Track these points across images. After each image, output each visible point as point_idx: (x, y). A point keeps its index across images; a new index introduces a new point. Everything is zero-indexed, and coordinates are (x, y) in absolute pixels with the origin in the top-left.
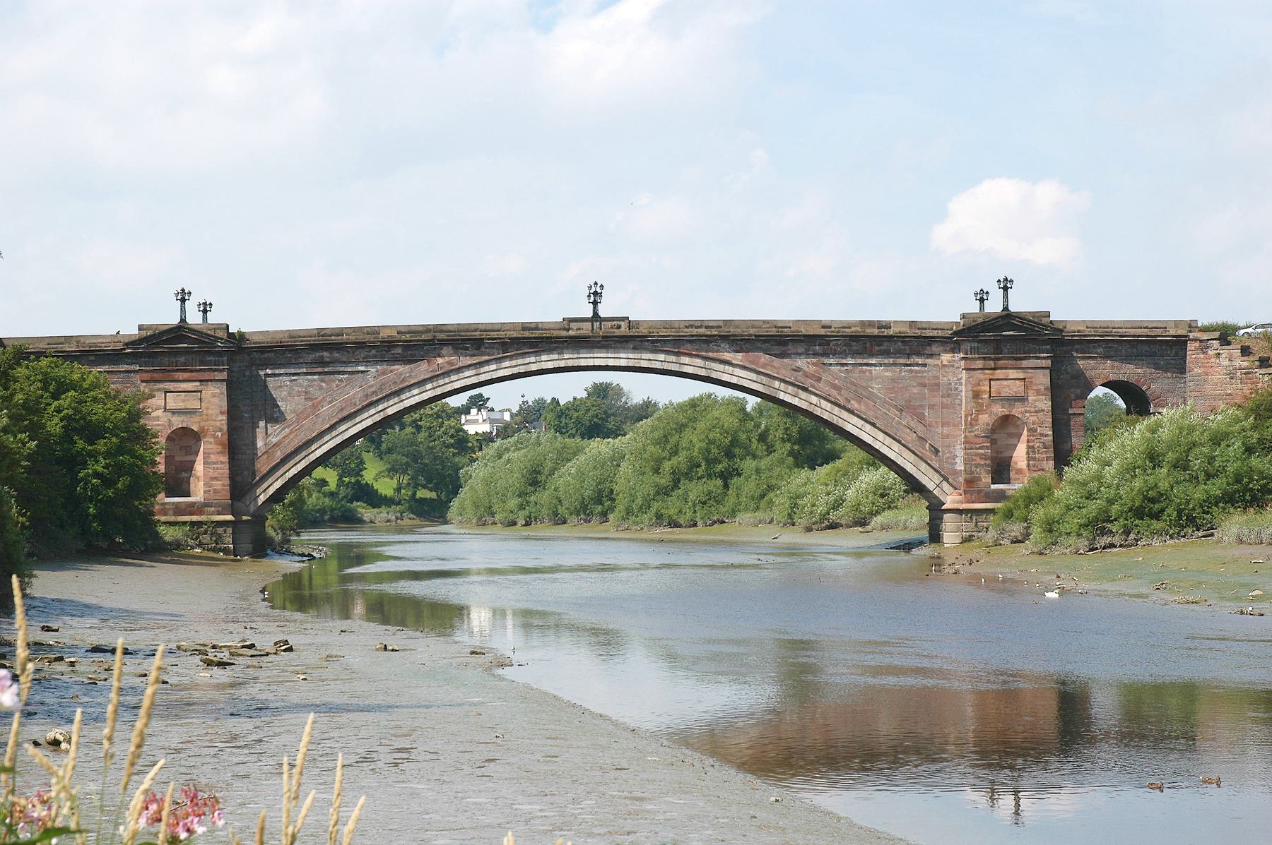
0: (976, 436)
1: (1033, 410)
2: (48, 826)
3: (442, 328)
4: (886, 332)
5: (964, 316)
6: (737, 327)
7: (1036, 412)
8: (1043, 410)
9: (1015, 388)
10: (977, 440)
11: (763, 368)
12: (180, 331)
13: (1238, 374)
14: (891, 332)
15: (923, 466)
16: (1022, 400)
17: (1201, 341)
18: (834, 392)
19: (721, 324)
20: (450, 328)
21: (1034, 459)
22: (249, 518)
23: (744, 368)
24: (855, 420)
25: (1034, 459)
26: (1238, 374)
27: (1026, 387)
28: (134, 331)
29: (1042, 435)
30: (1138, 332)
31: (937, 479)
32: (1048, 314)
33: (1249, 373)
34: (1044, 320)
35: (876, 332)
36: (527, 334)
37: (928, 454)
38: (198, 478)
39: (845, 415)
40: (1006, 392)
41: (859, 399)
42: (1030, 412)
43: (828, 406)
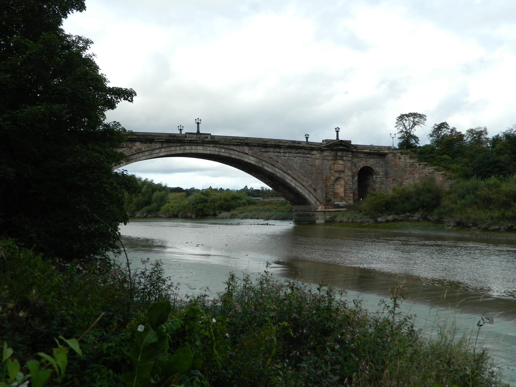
0: (330, 184)
1: (346, 175)
3: (136, 134)
4: (300, 145)
6: (250, 140)
7: (347, 176)
8: (349, 176)
9: (341, 168)
10: (330, 186)
11: (259, 156)
15: (311, 195)
17: (394, 153)
18: (283, 168)
19: (244, 139)
20: (139, 134)
21: (347, 193)
23: (252, 156)
24: (289, 178)
25: (347, 193)
26: (408, 165)
29: (349, 184)
31: (315, 200)
32: (350, 142)
33: (412, 164)
35: (297, 145)
36: (171, 138)
37: (312, 191)
38: (376, 266)
39: (286, 176)
40: (339, 169)
41: (291, 170)
42: (346, 176)
43: (281, 172)
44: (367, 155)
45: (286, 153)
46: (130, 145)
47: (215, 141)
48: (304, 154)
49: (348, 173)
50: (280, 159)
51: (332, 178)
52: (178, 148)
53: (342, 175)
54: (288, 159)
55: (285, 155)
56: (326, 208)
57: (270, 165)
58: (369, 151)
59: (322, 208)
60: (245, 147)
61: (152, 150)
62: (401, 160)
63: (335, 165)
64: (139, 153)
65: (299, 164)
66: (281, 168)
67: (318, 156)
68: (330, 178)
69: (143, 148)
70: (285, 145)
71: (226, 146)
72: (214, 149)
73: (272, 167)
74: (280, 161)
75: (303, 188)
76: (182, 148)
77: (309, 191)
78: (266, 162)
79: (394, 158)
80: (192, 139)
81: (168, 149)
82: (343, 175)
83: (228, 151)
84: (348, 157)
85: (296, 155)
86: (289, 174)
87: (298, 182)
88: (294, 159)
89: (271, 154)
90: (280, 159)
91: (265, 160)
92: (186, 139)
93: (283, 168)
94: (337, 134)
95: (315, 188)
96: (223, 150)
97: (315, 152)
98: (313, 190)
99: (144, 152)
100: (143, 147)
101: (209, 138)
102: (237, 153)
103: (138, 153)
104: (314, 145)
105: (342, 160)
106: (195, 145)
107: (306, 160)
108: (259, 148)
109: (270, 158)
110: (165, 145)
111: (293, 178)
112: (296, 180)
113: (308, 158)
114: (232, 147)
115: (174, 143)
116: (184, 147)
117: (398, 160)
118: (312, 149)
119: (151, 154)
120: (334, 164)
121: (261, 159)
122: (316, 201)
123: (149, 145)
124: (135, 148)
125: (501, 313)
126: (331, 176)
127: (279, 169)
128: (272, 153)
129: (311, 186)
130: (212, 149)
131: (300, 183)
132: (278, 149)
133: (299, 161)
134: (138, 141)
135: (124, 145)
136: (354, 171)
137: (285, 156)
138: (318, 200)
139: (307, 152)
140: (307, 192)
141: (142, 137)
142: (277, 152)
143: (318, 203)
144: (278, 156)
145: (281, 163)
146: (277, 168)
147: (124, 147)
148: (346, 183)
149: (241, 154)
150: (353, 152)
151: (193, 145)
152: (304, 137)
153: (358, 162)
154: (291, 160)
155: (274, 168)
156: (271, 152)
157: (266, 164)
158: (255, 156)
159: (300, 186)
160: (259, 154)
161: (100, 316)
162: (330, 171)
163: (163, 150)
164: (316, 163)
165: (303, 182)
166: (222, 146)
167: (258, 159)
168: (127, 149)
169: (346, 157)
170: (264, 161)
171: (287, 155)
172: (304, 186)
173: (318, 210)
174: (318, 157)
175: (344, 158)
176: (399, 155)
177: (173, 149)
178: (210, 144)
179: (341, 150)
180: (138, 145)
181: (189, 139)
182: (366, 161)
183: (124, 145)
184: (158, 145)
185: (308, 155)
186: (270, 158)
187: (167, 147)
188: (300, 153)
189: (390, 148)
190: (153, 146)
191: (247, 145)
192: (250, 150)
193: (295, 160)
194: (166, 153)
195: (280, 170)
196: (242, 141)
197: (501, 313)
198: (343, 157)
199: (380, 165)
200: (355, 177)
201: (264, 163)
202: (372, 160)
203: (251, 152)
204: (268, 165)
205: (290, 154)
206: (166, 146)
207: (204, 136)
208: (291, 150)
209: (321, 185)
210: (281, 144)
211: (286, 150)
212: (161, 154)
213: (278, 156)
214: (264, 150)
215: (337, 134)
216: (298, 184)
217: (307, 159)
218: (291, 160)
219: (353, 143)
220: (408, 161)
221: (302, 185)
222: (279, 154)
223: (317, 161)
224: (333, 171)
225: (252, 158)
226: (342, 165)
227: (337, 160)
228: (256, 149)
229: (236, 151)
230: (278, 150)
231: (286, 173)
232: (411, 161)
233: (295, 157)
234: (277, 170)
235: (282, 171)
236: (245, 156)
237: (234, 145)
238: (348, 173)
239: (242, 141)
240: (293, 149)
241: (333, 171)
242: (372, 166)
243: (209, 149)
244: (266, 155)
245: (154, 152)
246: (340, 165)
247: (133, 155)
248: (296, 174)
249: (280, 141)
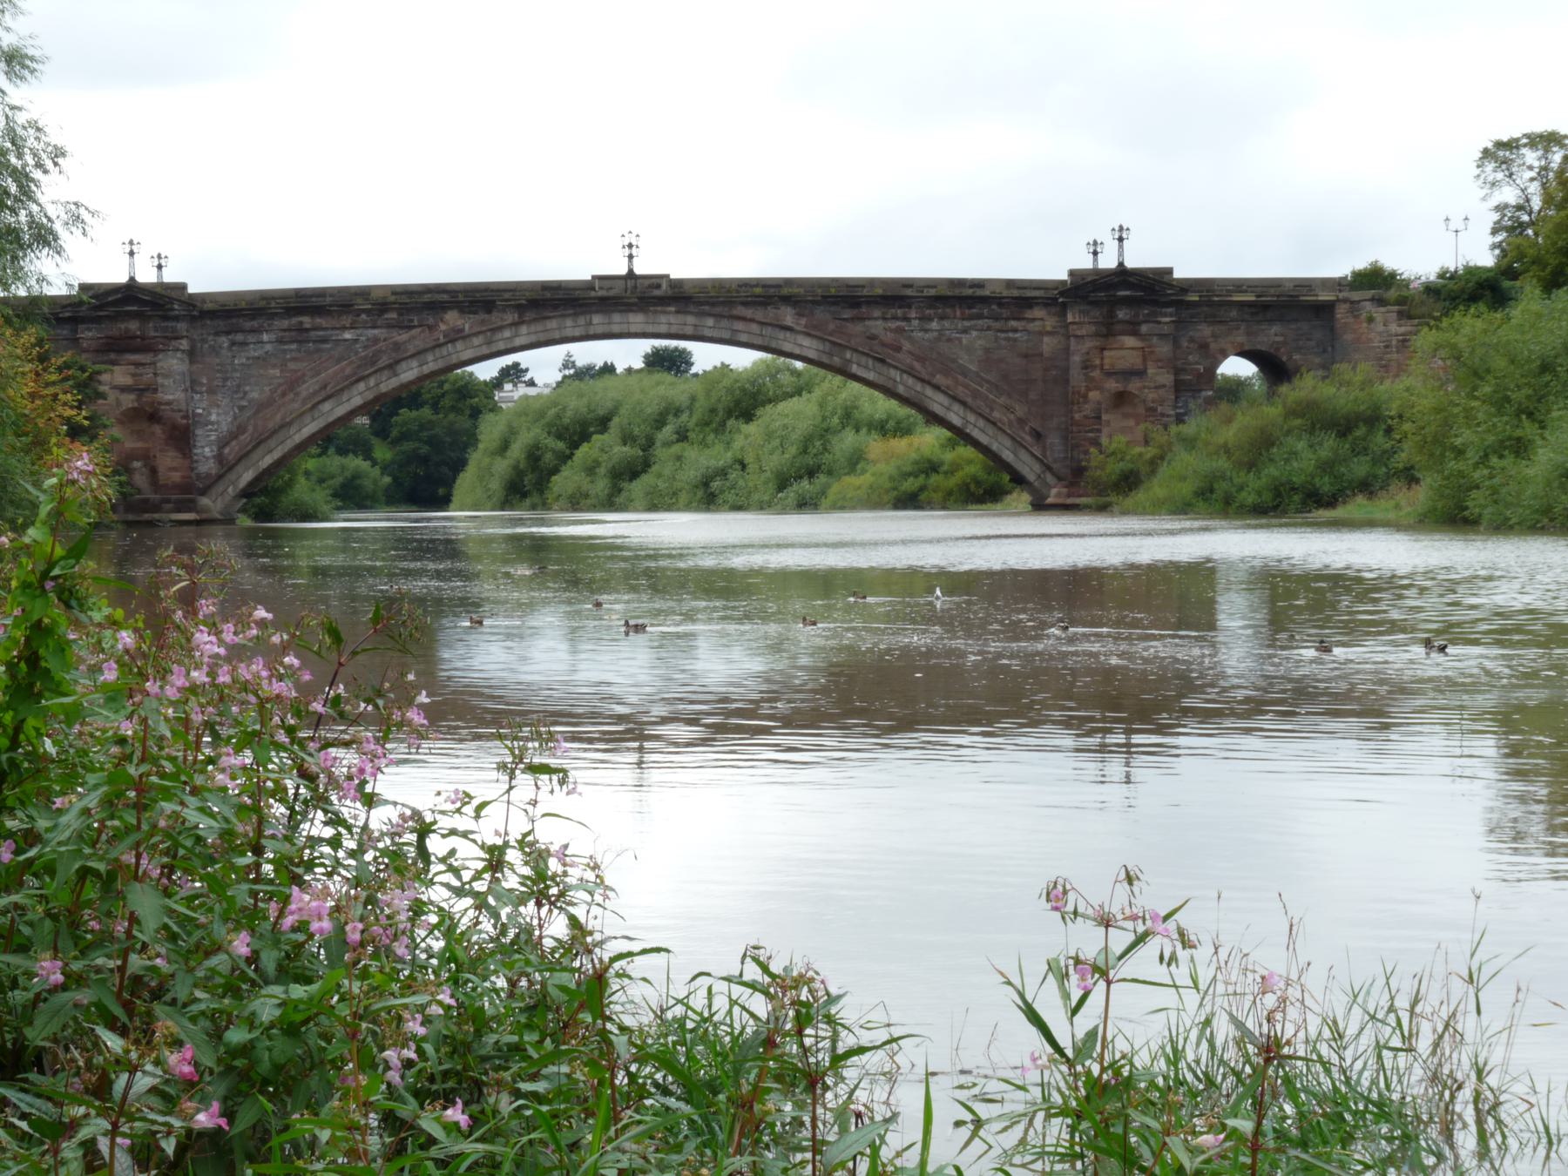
0: (1086, 417)
1: (1152, 385)
4: (979, 292)
5: (1072, 273)
7: (1156, 388)
8: (1164, 386)
11: (831, 334)
13: (1394, 343)
14: (987, 293)
17: (1352, 302)
18: (917, 365)
23: (809, 335)
24: (940, 398)
26: (1394, 343)
27: (1145, 360)
31: (1037, 467)
35: (970, 292)
36: (548, 295)
39: (929, 392)
40: (1121, 365)
41: (947, 372)
42: (1149, 388)
43: (910, 381)
44: (1253, 310)
45: (930, 319)
46: (431, 321)
48: (997, 319)
50: (910, 339)
51: (1094, 395)
52: (569, 322)
53: (1134, 386)
54: (938, 339)
55: (928, 327)
56: (1069, 496)
57: (870, 362)
58: (1253, 299)
59: (1058, 495)
60: (783, 308)
62: (1372, 325)
63: (1106, 353)
64: (456, 340)
65: (980, 353)
66: (912, 368)
67: (1050, 323)
68: (1085, 397)
69: (467, 326)
70: (925, 294)
71: (718, 310)
72: (680, 318)
73: (878, 365)
74: (907, 346)
75: (990, 430)
76: (582, 320)
77: (1013, 439)
78: (856, 351)
79: (1351, 320)
80: (612, 293)
81: (539, 327)
82: (1139, 385)
83: (725, 323)
84: (1159, 323)
85: (967, 324)
86: (937, 388)
87: (972, 409)
88: (960, 340)
89: (877, 326)
90: (910, 339)
91: (853, 343)
92: (593, 294)
93: (917, 365)
95: (1039, 429)
96: (710, 322)
97: (1038, 312)
98: (1030, 434)
99: (469, 336)
100: (467, 323)
101: (664, 286)
102: (755, 328)
103: (453, 341)
104: (1035, 289)
105: (1135, 333)
106: (621, 311)
107: (1008, 339)
108: (832, 309)
109: (873, 337)
110: (529, 316)
111: (955, 398)
112: (963, 403)
113: (1015, 331)
114: (740, 311)
115: (555, 307)
116: (588, 317)
117: (1365, 325)
119: (489, 343)
120: (1103, 349)
121: (839, 341)
122: (1043, 472)
123: (482, 316)
124: (443, 327)
125: (544, 530)
126: (1088, 389)
127: (903, 371)
128: (879, 323)
129: (1022, 422)
130: (673, 319)
131: (981, 415)
132: (900, 307)
133: (979, 342)
134: (450, 308)
135: (412, 321)
136: (1198, 370)
137: (926, 331)
138: (1049, 468)
139: (1005, 313)
140: (1008, 443)
141: (461, 298)
142: (895, 318)
143: (1050, 478)
144: (900, 330)
145: (910, 352)
146: (896, 368)
147: (414, 327)
149: (768, 331)
150: (1180, 304)
151: (613, 311)
152: (1084, 249)
153: (1214, 336)
154: (949, 340)
155: (884, 369)
156: (876, 319)
157: (855, 357)
158: (818, 334)
159: (981, 423)
160: (831, 326)
162: (1085, 374)
163: (524, 329)
164: (1045, 347)
165: (992, 410)
166: (707, 308)
167: (827, 344)
168: (423, 331)
169: (1151, 325)
170: (846, 347)
171: (934, 325)
172: (994, 424)
173: (1050, 500)
174: (1049, 329)
175: (1144, 328)
176: (1368, 309)
177: (552, 324)
178: (669, 305)
180: (452, 318)
181: (601, 293)
182: (1248, 334)
183: (412, 321)
184: (510, 317)
185: (1013, 323)
186: (868, 338)
187: (535, 320)
188: (980, 317)
189: (1340, 285)
190: (496, 318)
191: (787, 300)
192: (800, 315)
193: (964, 341)
194: (533, 338)
195: (905, 376)
196: (772, 290)
197: (544, 530)
198: (1139, 324)
199: (1313, 343)
200: (1200, 391)
201: (848, 355)
202: (1275, 328)
203: (803, 321)
204: (863, 360)
205: (946, 324)
206: (534, 316)
207: (647, 282)
208: (948, 310)
209: (1063, 419)
210: (909, 292)
211: (928, 312)
213: (900, 330)
214: (847, 314)
216: (971, 418)
217: (1011, 335)
218: (949, 340)
219: (1178, 274)
220: (1394, 328)
221: (988, 420)
222: (903, 324)
223: (1046, 339)
224: (1096, 374)
225: (806, 342)
226: (1135, 353)
227: (1114, 335)
228: (821, 314)
229: (752, 320)
230: (900, 312)
231: (929, 383)
232: (1402, 329)
233: (965, 331)
234: (894, 373)
235: (914, 376)
236: (781, 335)
237: (745, 304)
239: (772, 290)
240: (953, 306)
241: (1096, 374)
242: (1278, 349)
243: (663, 319)
244: (858, 328)
245: (499, 336)
246: (1126, 351)
247: (440, 346)
248: (966, 386)
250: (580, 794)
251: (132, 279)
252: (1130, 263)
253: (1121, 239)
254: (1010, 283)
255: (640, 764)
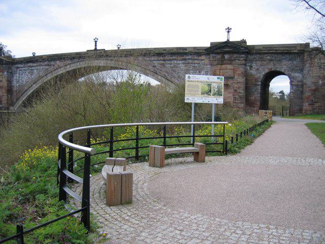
2: (298, 60)
5: (211, 43)
8: (240, 82)
12: (227, 44)
13: (323, 66)
14: (187, 51)
16: (232, 78)
22: (154, 82)
26: (323, 66)
27: (234, 73)
28: (209, 45)
29: (239, 93)
30: (284, 49)
34: (243, 44)
35: (182, 51)
47: (129, 53)
49: (238, 79)
61: (66, 66)
82: (231, 82)
94: (96, 44)
118: (186, 54)
148: (236, 91)
161: (315, 123)
179: (228, 52)
212: (38, 70)
215: (96, 44)
238: (238, 79)
249: (165, 49)
250: (229, 30)
251: (228, 40)
252: (231, 40)
253: (228, 32)
254: (195, 48)
255: (137, 139)
